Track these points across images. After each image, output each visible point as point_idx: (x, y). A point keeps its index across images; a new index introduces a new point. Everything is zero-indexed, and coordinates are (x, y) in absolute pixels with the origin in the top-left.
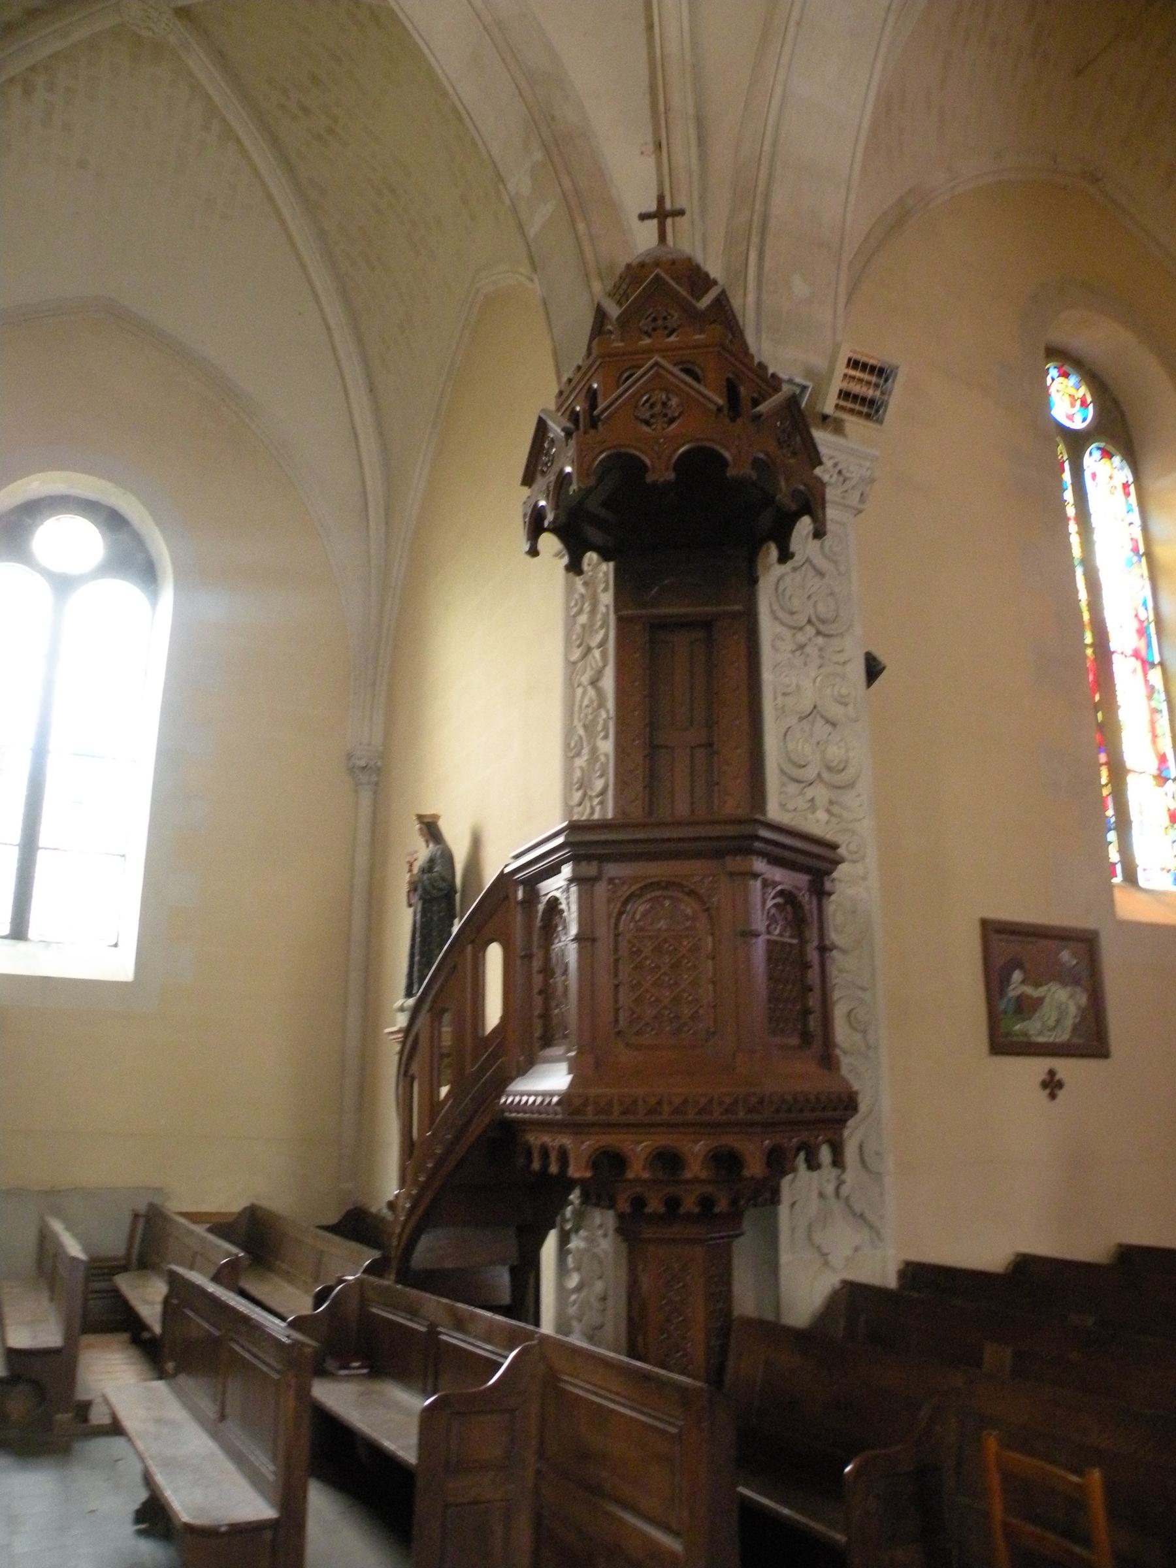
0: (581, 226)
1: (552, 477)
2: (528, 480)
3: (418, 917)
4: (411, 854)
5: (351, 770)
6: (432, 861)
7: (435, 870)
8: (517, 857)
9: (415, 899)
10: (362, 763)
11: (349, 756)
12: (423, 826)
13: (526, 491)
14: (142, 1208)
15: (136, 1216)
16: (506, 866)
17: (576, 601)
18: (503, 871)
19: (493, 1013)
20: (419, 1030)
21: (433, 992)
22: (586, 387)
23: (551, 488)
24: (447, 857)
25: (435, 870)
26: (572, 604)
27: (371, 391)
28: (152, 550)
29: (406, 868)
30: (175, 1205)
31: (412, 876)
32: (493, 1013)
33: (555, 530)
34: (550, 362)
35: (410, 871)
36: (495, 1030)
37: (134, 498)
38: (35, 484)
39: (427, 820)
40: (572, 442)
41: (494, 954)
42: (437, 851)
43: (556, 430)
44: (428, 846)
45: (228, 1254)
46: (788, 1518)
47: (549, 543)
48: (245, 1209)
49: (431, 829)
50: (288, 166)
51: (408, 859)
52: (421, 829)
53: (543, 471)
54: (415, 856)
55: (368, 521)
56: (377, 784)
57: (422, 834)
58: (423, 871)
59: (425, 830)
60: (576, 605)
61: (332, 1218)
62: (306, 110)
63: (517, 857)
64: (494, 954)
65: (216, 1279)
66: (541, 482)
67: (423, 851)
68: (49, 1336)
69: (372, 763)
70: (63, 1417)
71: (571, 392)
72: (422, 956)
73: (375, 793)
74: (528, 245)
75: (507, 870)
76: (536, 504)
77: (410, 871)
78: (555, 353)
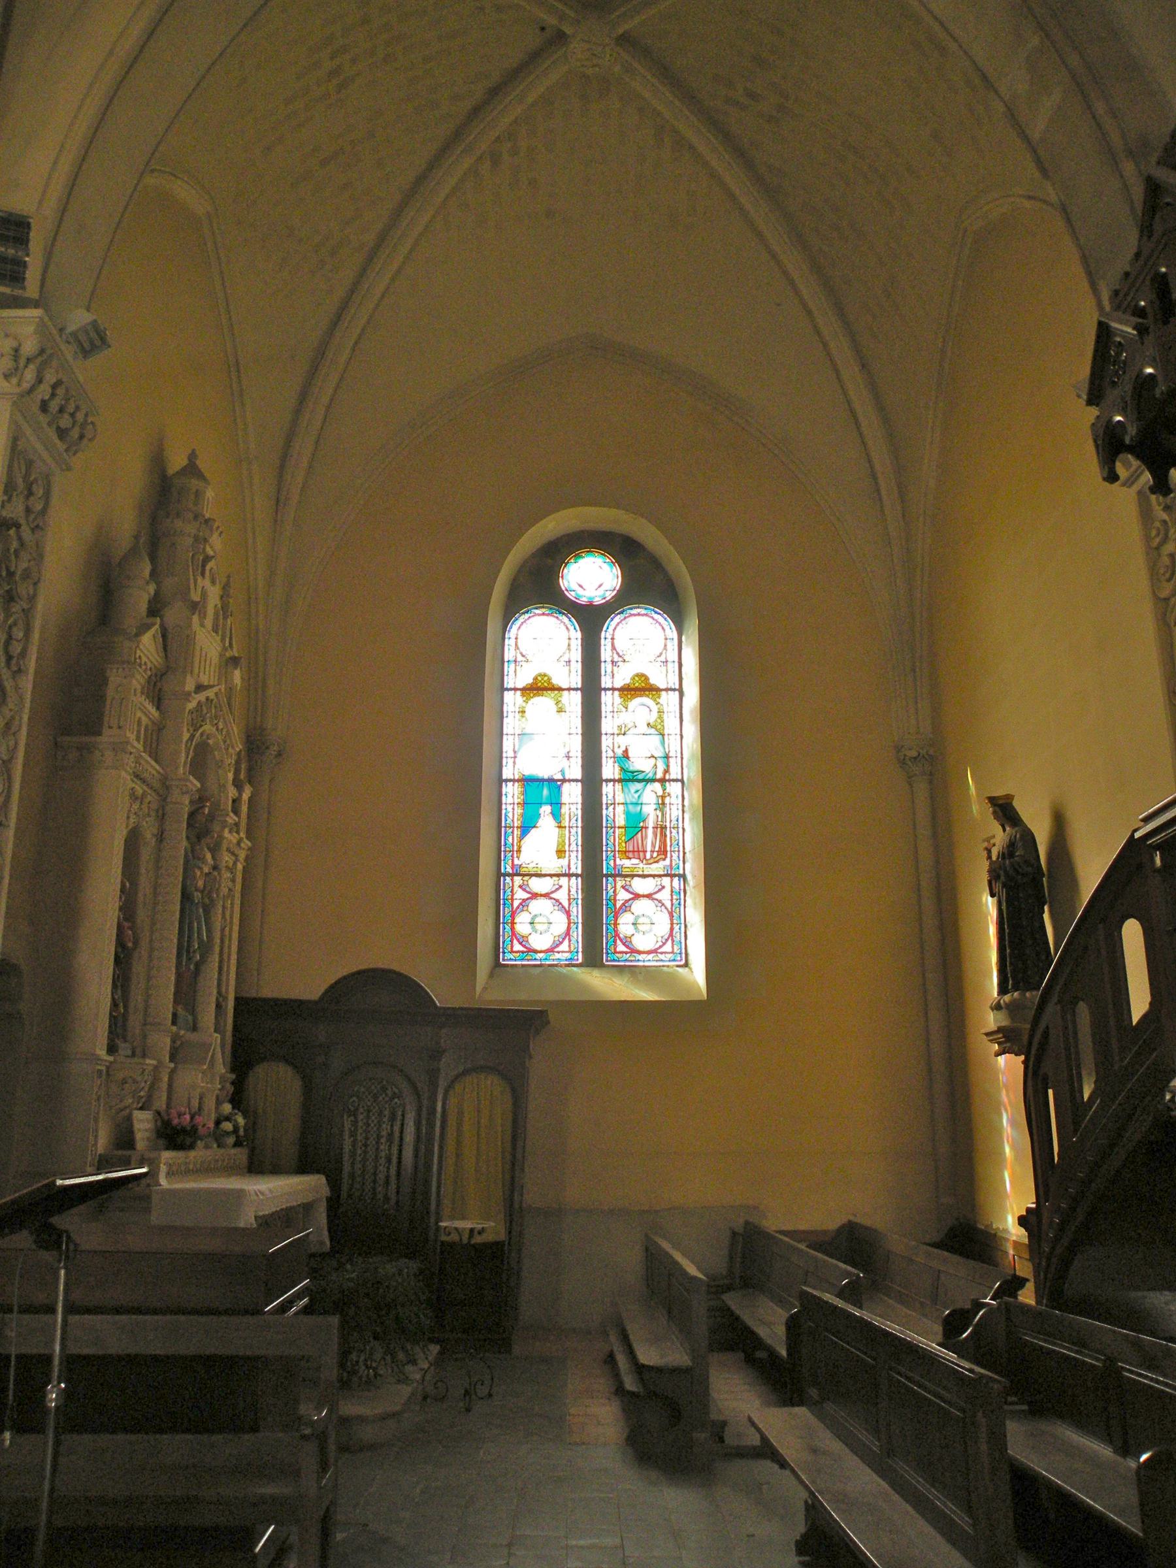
0: (1100, 108)
1: (1128, 387)
2: (1094, 397)
3: (1004, 907)
4: (988, 840)
5: (902, 763)
6: (1011, 845)
7: (1017, 854)
8: (1147, 820)
9: (998, 887)
10: (914, 753)
11: (898, 749)
12: (997, 809)
13: (1094, 412)
14: (739, 1226)
15: (734, 1234)
16: (1136, 830)
17: (1158, 529)
18: (1132, 835)
19: (1139, 1003)
20: (1047, 1027)
21: (1061, 981)
22: (1153, 272)
23: (1128, 399)
24: (1029, 839)
25: (1017, 854)
26: (1154, 533)
27: (863, 366)
28: (669, 568)
29: (985, 854)
30: (772, 1223)
31: (992, 863)
32: (1139, 1003)
33: (1137, 450)
34: (1078, 270)
35: (989, 857)
36: (1145, 1017)
37: (1142, 187)
38: (551, 526)
39: (1001, 802)
40: (1150, 339)
41: (1132, 933)
42: (1016, 832)
43: (1125, 328)
44: (1004, 830)
45: (848, 1274)
46: (1101, 1512)
47: (1127, 465)
48: (843, 1226)
49: (1005, 810)
50: (741, 155)
51: (986, 844)
52: (994, 813)
53: (1114, 382)
54: (992, 841)
55: (880, 499)
56: (931, 774)
57: (996, 817)
58: (1003, 856)
59: (1000, 814)
60: (1158, 535)
61: (937, 1237)
62: (752, 95)
63: (1147, 820)
64: (1132, 933)
65: (840, 1295)
66: (1112, 395)
67: (1000, 836)
68: (676, 1356)
69: (923, 752)
70: (701, 1436)
71: (1130, 289)
72: (1012, 950)
73: (931, 782)
74: (1034, 151)
75: (1137, 835)
76: (1110, 420)
77: (989, 857)
78: (1085, 260)
